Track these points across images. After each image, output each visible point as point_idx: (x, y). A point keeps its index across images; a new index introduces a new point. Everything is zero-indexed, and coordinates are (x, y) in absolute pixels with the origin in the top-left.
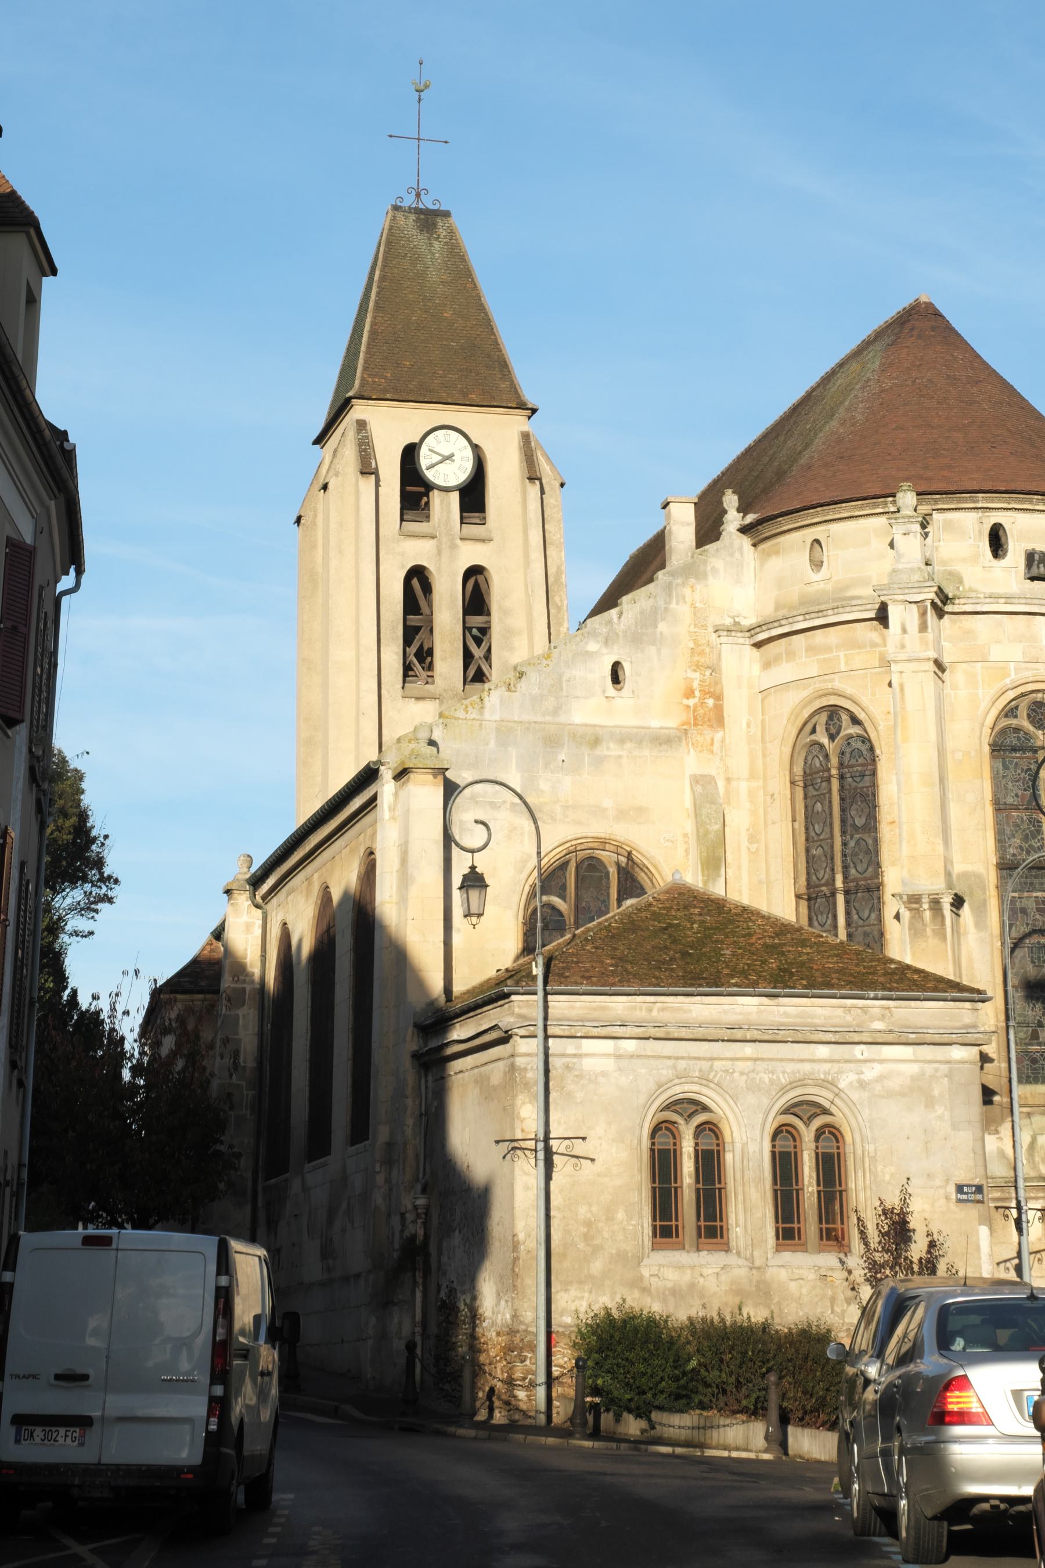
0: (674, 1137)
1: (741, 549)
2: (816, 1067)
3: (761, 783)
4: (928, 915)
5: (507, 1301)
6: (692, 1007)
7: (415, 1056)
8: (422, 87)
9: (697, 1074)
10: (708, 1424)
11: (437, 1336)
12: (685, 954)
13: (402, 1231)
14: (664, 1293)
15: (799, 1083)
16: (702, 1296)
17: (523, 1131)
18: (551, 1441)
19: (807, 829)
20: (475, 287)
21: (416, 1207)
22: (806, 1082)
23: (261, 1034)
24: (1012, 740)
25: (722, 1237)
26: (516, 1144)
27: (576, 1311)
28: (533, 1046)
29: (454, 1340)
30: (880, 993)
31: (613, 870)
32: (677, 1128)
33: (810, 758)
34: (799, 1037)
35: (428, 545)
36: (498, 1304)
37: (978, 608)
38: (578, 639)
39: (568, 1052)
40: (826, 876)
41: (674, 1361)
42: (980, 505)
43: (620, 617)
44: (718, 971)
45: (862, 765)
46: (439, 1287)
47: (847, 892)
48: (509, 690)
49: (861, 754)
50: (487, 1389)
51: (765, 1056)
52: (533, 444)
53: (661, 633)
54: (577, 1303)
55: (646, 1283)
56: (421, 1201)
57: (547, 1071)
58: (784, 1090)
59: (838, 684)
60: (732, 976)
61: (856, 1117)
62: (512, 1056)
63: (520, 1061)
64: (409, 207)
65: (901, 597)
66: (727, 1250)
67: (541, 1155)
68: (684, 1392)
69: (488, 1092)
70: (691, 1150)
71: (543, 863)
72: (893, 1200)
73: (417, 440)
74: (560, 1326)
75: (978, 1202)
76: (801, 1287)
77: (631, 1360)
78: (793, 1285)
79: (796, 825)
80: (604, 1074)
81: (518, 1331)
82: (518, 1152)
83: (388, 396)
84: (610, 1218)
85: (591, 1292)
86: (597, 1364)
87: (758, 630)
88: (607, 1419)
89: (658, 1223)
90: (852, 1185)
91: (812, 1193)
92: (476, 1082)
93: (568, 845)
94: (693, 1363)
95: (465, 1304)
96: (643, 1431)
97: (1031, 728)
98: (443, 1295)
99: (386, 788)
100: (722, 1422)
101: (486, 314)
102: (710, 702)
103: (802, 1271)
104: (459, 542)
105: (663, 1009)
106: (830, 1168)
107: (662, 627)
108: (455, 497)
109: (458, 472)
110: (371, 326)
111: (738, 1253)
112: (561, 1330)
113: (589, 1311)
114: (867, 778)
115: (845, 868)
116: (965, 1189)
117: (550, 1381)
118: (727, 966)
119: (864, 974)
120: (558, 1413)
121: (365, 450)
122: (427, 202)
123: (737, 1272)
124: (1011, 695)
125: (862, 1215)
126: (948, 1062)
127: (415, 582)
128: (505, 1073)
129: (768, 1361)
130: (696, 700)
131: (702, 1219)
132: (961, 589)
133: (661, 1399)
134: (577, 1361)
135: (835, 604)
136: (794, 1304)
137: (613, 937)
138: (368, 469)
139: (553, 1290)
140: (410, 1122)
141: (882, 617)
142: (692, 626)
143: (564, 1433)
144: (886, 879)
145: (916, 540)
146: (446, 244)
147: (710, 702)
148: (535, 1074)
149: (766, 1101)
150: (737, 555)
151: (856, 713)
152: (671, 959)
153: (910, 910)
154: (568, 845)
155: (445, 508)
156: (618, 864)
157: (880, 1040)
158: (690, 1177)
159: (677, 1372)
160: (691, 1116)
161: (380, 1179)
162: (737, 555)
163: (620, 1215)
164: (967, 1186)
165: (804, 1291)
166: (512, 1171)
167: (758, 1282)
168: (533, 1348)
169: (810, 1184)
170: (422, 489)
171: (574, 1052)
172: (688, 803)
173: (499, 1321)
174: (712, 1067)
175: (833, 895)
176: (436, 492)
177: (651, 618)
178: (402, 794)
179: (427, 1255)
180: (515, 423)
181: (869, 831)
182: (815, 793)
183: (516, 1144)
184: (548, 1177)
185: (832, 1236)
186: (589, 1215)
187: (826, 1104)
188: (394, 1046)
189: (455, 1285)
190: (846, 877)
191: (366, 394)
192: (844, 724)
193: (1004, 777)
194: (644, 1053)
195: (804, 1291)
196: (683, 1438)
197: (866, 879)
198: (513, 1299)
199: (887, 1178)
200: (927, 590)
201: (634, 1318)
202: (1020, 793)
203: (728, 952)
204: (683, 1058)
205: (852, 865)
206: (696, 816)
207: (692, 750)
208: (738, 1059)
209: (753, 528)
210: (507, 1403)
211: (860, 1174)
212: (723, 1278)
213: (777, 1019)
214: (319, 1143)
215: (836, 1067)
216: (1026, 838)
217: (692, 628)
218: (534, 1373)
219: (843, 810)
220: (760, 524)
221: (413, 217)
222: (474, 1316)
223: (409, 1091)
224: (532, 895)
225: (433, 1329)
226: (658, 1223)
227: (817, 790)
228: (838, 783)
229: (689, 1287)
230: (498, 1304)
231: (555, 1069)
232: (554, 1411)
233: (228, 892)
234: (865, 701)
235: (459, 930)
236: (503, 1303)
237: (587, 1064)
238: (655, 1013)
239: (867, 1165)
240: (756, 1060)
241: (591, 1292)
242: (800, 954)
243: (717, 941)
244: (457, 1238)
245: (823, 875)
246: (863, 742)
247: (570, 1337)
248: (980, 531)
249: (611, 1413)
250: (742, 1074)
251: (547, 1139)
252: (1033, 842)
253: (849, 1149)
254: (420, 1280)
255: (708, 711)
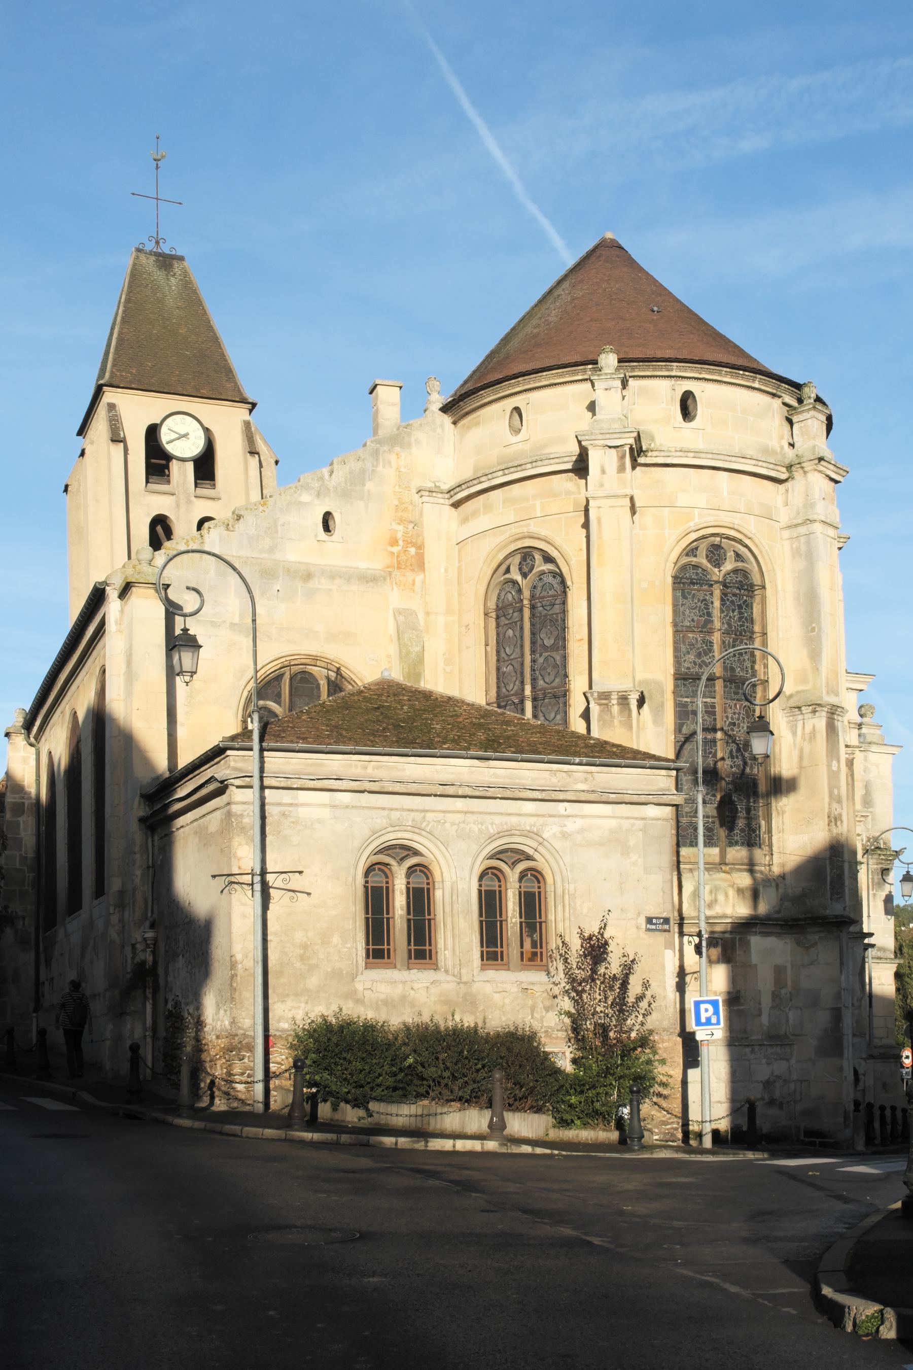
0: (387, 877)
1: (442, 426)
2: (523, 820)
3: (456, 618)
4: (616, 709)
5: (225, 1011)
6: (406, 766)
7: (142, 820)
8: (159, 157)
9: (410, 823)
10: (425, 1112)
11: (165, 1038)
12: (397, 726)
13: (133, 958)
14: (377, 1004)
15: (506, 833)
16: (412, 1006)
17: (239, 868)
18: (269, 1132)
19: (498, 652)
20: (205, 314)
21: (145, 939)
22: (513, 832)
23: (38, 834)
24: (691, 573)
25: (431, 958)
26: (233, 879)
27: (294, 1018)
28: (251, 795)
29: (179, 1041)
30: (585, 760)
31: (323, 683)
32: (390, 869)
33: (503, 593)
34: (508, 794)
35: (169, 500)
36: (218, 1012)
37: (669, 461)
38: (292, 491)
39: (284, 801)
40: (516, 688)
41: (392, 1060)
42: (673, 373)
43: (331, 475)
44: (430, 739)
45: (552, 596)
46: (166, 1001)
47: (534, 699)
48: (228, 529)
49: (551, 586)
50: (208, 1081)
51: (475, 810)
52: (253, 429)
53: (369, 491)
54: (294, 1012)
55: (360, 996)
56: (150, 935)
57: (263, 817)
58: (492, 838)
59: (533, 527)
60: (444, 743)
61: (557, 862)
62: (228, 804)
63: (235, 808)
64: (151, 251)
65: (602, 442)
66: (436, 968)
67: (258, 887)
68: (401, 1085)
69: (205, 838)
70: (404, 887)
71: (259, 674)
72: (592, 928)
73: (158, 422)
74: (278, 1030)
75: (665, 931)
76: (504, 998)
77: (344, 1057)
78: (497, 998)
79: (489, 648)
80: (319, 821)
81: (237, 1035)
82: (236, 886)
83: (133, 386)
84: (325, 942)
85: (307, 1003)
86: (314, 1062)
87: (458, 489)
88: (324, 1110)
89: (371, 947)
90: (551, 917)
91: (515, 923)
92: (195, 833)
93: (284, 660)
94: (411, 1060)
95: (189, 1014)
96: (360, 1119)
97: (709, 565)
98: (170, 1006)
99: (112, 607)
100: (439, 1111)
101: (215, 334)
102: (413, 550)
103: (505, 986)
104: (194, 499)
105: (378, 768)
106: (532, 905)
107: (369, 485)
108: (190, 466)
109: (194, 447)
110: (119, 335)
111: (447, 971)
112: (278, 1034)
113: (306, 1018)
114: (556, 607)
115: (534, 680)
116: (654, 921)
117: (268, 1075)
118: (438, 736)
119: (567, 746)
120: (275, 1101)
121: (115, 425)
122: (165, 249)
123: (445, 986)
124: (694, 536)
125: (567, 939)
126: (643, 819)
127: (159, 529)
128: (222, 821)
129: (483, 1059)
130: (400, 548)
131: (412, 943)
132: (653, 445)
133: (378, 1092)
134: (295, 1063)
135: (534, 459)
136: (498, 1012)
137: (327, 711)
138: (117, 438)
139: (270, 1001)
140: (139, 873)
141: (581, 468)
142: (397, 487)
143: (283, 1121)
144: (572, 686)
145: (616, 393)
146: (181, 280)
147: (413, 550)
148: (251, 818)
149: (475, 848)
150: (439, 430)
151: (549, 552)
152: (384, 729)
153: (600, 705)
154: (284, 660)
155: (182, 474)
156: (328, 678)
157: (583, 799)
158: (402, 910)
159: (394, 1069)
160: (402, 859)
161: (114, 919)
162: (439, 430)
163: (336, 939)
164: (656, 918)
165: (507, 1001)
166: (229, 903)
167: (465, 995)
168: (250, 1048)
169: (513, 916)
170: (163, 462)
171: (291, 801)
172: (392, 629)
173: (218, 1027)
174: (424, 818)
175: (522, 702)
176: (174, 460)
177: (360, 478)
178: (127, 609)
179: (156, 977)
180: (240, 413)
181: (558, 650)
182: (507, 622)
183: (233, 879)
184: (265, 907)
185: (535, 957)
186: (305, 940)
187: (530, 852)
188: (124, 812)
189: (180, 998)
190: (533, 688)
191: (115, 383)
192: (537, 562)
193: (682, 605)
194: (359, 804)
195: (507, 1001)
196: (400, 1124)
197: (553, 688)
198: (231, 1008)
199: (585, 911)
200: (627, 435)
201: (349, 1024)
202: (696, 619)
203: (438, 726)
204: (396, 809)
205: (540, 677)
206: (399, 639)
207: (395, 588)
208: (449, 812)
209: (454, 405)
210: (227, 1093)
211: (560, 908)
212: (433, 991)
213: (487, 779)
214: (75, 904)
215: (541, 820)
216: (699, 655)
217: (397, 488)
218: (252, 1069)
219: (533, 634)
220: (462, 400)
221: (153, 258)
222: (199, 1024)
223: (137, 849)
224: (248, 701)
225: (162, 1033)
226: (371, 947)
227: (509, 620)
228: (532, 609)
229: (399, 998)
230: (218, 1012)
231: (272, 816)
232: (272, 1099)
233: (7, 735)
234: (558, 540)
235: (183, 724)
236: (222, 1012)
237: (303, 812)
238: (370, 770)
239: (567, 901)
240: (466, 813)
241: (307, 1003)
242: (505, 731)
243: (427, 719)
244: (181, 962)
245: (513, 687)
246: (554, 577)
247: (287, 1040)
248: (672, 397)
249: (329, 1104)
250: (453, 824)
251: (264, 872)
252: (705, 659)
253: (550, 888)
254: (150, 996)
255: (410, 557)
